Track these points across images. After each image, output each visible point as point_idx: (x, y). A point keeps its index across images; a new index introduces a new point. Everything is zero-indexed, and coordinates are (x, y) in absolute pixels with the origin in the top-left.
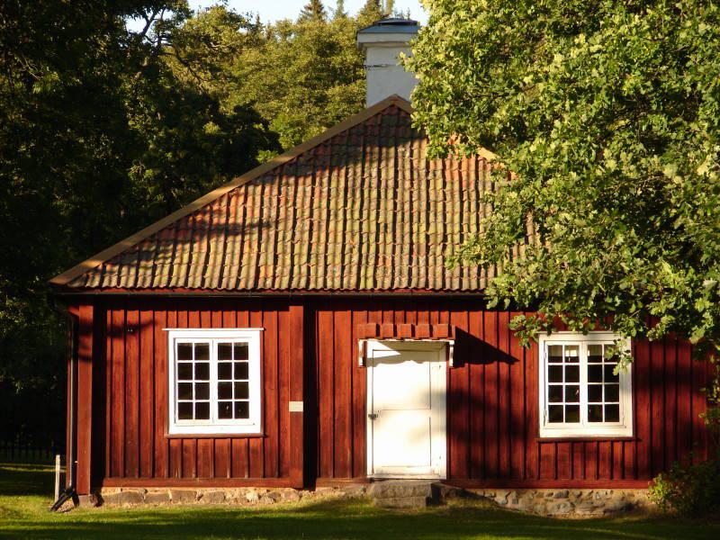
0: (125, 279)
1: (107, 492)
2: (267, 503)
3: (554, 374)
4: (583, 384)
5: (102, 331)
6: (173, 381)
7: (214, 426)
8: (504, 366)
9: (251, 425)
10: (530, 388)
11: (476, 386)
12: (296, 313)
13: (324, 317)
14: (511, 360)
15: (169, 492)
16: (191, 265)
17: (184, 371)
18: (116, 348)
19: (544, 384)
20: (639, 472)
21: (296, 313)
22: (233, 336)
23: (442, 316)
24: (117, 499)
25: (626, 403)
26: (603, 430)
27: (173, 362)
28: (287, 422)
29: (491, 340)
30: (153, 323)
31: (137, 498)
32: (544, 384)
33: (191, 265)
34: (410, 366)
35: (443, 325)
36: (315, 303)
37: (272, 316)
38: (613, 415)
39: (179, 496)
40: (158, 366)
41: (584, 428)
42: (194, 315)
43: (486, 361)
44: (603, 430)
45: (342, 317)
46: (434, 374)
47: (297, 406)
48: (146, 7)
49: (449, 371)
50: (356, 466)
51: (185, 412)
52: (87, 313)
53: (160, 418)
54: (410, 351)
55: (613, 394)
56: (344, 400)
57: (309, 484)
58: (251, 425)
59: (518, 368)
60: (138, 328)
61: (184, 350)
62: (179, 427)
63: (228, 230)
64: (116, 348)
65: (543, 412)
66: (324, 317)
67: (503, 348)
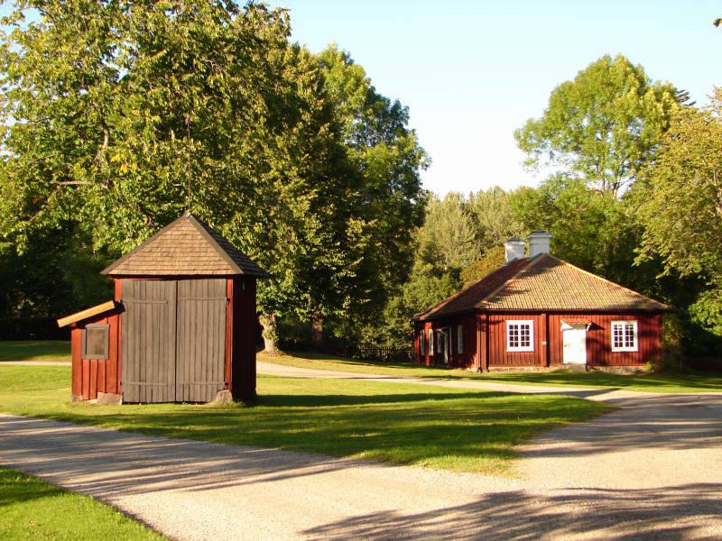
0: (494, 306)
1: (490, 368)
2: (536, 371)
3: (616, 333)
4: (624, 336)
5: (488, 322)
6: (508, 336)
7: (520, 349)
8: (602, 331)
9: (531, 348)
10: (609, 338)
11: (594, 337)
12: (543, 316)
13: (551, 317)
14: (603, 329)
15: (508, 368)
16: (510, 302)
17: (511, 333)
18: (492, 327)
19: (613, 336)
20: (643, 361)
21: (543, 316)
22: (525, 322)
23: (187, 306)
24: (493, 370)
25: (635, 341)
26: (526, 349)
27: (508, 330)
28: (541, 349)
29: (598, 324)
30: (503, 321)
31: (499, 370)
32: (613, 336)
33: (510, 302)
34: (575, 330)
35: (587, 320)
36: (549, 312)
37: (536, 317)
38: (632, 345)
39: (511, 369)
40: (504, 332)
41: (624, 349)
42: (528, 316)
43: (597, 329)
44: (526, 349)
45: (556, 317)
46: (581, 334)
47: (545, 343)
48: (337, 211)
49: (587, 333)
50: (561, 360)
51: (511, 345)
52: (484, 317)
53: (504, 346)
54: (576, 326)
55: (632, 339)
56: (557, 341)
57: (548, 365)
58: (531, 348)
59: (606, 331)
60: (498, 322)
61: (511, 327)
62: (510, 349)
63: (519, 292)
64: (492, 327)
65: (613, 345)
66: (551, 317)
67: (601, 325)
